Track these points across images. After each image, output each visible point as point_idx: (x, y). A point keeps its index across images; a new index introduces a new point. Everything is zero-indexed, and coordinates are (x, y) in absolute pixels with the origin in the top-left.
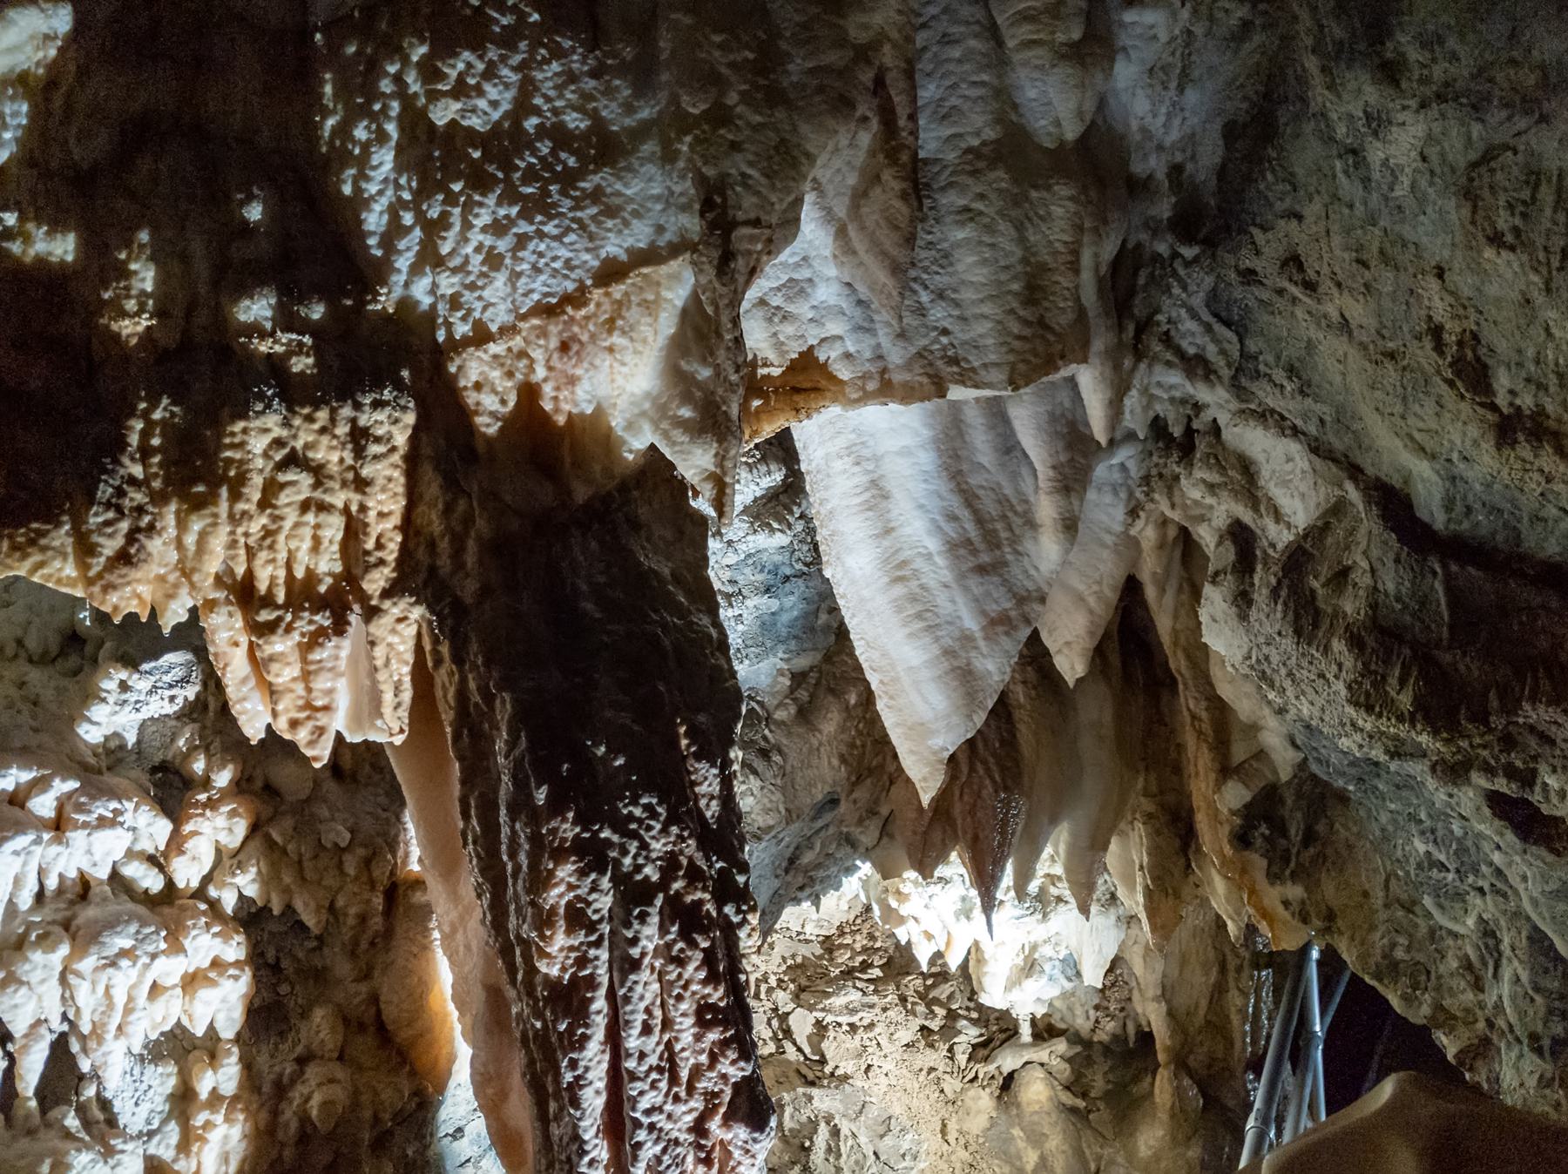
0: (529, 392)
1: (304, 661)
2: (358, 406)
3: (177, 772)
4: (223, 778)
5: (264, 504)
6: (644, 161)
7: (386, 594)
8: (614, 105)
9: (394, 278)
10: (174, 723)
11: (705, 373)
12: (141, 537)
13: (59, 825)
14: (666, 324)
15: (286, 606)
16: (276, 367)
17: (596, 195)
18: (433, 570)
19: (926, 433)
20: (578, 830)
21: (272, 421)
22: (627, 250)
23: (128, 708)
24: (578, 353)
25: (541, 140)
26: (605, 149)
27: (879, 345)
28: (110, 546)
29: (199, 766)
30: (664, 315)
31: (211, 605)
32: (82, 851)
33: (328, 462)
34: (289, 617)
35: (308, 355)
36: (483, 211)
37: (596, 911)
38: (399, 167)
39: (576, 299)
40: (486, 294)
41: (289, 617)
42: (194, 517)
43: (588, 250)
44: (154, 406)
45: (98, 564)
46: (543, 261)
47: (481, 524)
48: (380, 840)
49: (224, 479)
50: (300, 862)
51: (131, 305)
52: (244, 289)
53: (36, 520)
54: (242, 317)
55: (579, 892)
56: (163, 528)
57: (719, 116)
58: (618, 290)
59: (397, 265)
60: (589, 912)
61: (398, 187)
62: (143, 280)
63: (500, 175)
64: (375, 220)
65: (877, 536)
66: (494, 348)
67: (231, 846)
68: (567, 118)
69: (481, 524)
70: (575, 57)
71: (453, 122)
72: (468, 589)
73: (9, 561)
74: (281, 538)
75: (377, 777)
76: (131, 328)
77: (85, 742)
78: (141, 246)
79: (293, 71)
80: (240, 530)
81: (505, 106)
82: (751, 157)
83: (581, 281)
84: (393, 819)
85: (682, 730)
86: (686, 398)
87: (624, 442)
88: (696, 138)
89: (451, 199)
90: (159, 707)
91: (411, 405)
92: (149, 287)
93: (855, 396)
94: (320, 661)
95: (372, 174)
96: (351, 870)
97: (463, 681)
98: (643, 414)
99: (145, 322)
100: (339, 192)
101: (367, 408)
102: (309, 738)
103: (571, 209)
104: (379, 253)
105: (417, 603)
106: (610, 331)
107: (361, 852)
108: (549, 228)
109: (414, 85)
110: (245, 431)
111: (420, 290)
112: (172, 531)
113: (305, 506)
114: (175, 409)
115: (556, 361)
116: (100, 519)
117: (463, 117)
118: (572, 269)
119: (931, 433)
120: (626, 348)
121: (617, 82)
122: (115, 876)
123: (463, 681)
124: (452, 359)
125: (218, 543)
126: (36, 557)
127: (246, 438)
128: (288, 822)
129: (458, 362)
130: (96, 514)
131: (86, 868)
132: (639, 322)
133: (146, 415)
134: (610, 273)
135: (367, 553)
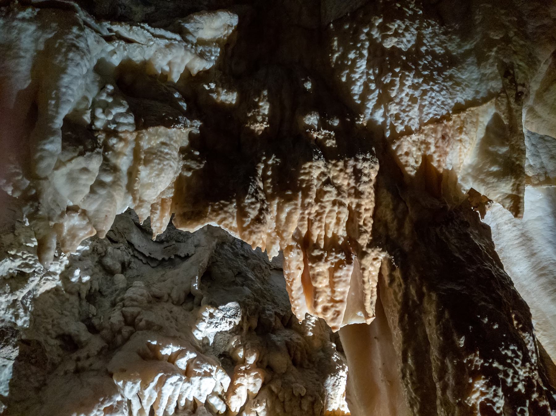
0: (427, 159)
1: (332, 276)
2: (357, 160)
3: (231, 358)
4: (251, 360)
5: (317, 200)
6: (469, 65)
7: (369, 246)
8: (453, 45)
9: (367, 111)
10: (228, 335)
11: (504, 150)
12: (264, 212)
13: (188, 374)
14: (479, 133)
15: (324, 250)
16: (320, 144)
17: (451, 78)
18: (388, 237)
19: (549, 210)
20: (482, 361)
21: (321, 163)
22: (464, 100)
23: (213, 326)
24: (448, 141)
25: (428, 55)
26: (451, 61)
27: (542, 163)
28: (253, 214)
29: (241, 354)
30: (480, 128)
31: (290, 248)
32: (196, 388)
33: (343, 185)
34: (326, 255)
35: (333, 140)
36: (409, 79)
37: (498, 408)
38: (369, 66)
39: (447, 117)
40: (410, 114)
41: (326, 255)
42: (287, 205)
43: (450, 98)
44: (269, 158)
45: (248, 221)
46: (434, 100)
47: (411, 213)
48: (317, 394)
49: (301, 189)
50: (283, 402)
51: (260, 118)
52: (307, 111)
53: (223, 200)
54: (307, 122)
55: (488, 396)
56: (271, 211)
57: (507, 40)
58: (463, 115)
59: (368, 106)
60: (495, 409)
61: (368, 74)
62: (265, 109)
63: (413, 67)
64: (357, 89)
65: (528, 257)
66: (414, 137)
67: (254, 393)
68: (436, 49)
69: (411, 213)
70: (437, 28)
71: (393, 47)
72: (407, 245)
73: (211, 216)
74: (325, 216)
75: (311, 366)
76: (259, 127)
77: (196, 338)
78: (264, 97)
79: (320, 39)
80: (307, 212)
81: (413, 43)
82: (521, 58)
83: (448, 110)
84: (321, 385)
85: (513, 316)
86: (494, 162)
87: (461, 186)
88: (499, 48)
89: (395, 75)
90: (225, 327)
91: (378, 161)
92: (266, 112)
93: (536, 182)
94: (340, 277)
95: (357, 70)
96: (305, 408)
97: (407, 289)
98: (468, 174)
99: (265, 126)
100: (340, 80)
101: (361, 161)
102: (332, 316)
103: (442, 81)
104: (359, 102)
105: (383, 251)
106: (461, 133)
107: (310, 399)
108: (436, 87)
109: (376, 34)
110: (310, 167)
111: (379, 117)
112: (275, 213)
113: (334, 203)
114: (278, 160)
115: (440, 143)
116: (250, 201)
117: (398, 44)
118: (445, 105)
119: (552, 210)
120: (466, 141)
121: (454, 37)
122: (207, 404)
123: (407, 289)
124: (394, 143)
125: (296, 217)
126: (222, 216)
127: (310, 170)
128: (279, 382)
129: (398, 143)
130: (248, 199)
131: (196, 396)
132: (470, 130)
133: (265, 162)
134: (459, 109)
135: (360, 226)
